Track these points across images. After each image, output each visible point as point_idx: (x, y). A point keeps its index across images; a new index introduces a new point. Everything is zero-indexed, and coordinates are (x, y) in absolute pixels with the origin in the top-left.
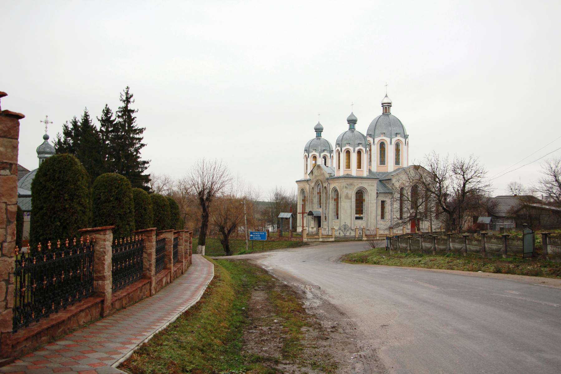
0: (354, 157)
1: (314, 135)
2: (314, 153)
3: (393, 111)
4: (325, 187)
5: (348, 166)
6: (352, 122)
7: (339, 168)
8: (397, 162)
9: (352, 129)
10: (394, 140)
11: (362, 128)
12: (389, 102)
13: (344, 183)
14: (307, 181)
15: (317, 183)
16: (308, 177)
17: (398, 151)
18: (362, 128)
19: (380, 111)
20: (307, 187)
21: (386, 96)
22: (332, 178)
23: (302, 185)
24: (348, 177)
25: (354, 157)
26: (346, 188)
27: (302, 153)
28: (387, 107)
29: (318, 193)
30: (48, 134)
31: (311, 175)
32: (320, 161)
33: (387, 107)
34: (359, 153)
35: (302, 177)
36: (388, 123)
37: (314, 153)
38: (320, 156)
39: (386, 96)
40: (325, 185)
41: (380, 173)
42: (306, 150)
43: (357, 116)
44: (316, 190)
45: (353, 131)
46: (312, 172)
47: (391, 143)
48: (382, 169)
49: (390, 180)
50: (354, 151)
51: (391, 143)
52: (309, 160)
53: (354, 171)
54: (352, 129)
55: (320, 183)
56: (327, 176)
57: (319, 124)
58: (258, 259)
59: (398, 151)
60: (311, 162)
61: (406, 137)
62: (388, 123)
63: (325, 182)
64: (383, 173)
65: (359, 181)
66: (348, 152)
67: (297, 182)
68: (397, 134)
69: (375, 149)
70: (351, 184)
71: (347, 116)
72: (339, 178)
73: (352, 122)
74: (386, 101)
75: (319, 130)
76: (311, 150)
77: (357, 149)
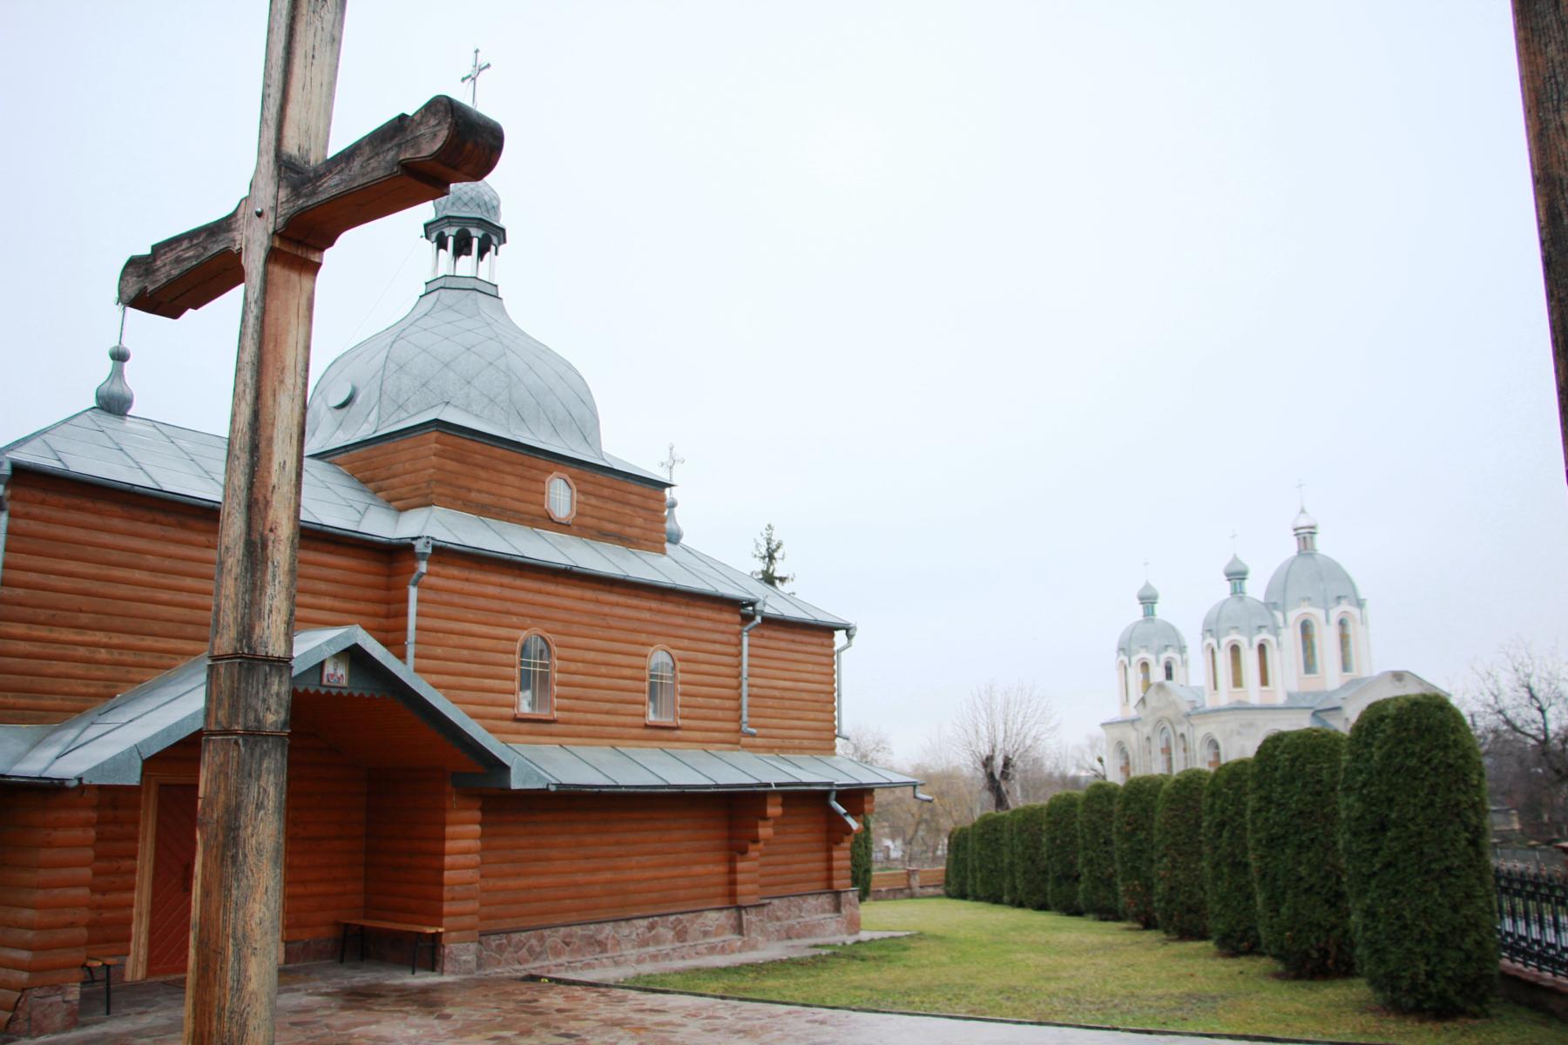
0: (1250, 659)
1: (1138, 612)
2: (1144, 655)
3: (1322, 544)
4: (1182, 736)
5: (1237, 682)
6: (1237, 576)
7: (1216, 688)
8: (1346, 667)
9: (1237, 592)
10: (1335, 614)
11: (1256, 588)
12: (1311, 523)
13: (1233, 722)
14: (1133, 722)
15: (1160, 725)
16: (1133, 713)
17: (1344, 640)
18: (1256, 588)
19: (1291, 547)
20: (1133, 738)
21: (1303, 511)
22: (1196, 713)
23: (1117, 733)
24: (1240, 708)
25: (1250, 659)
26: (1239, 733)
27: (1112, 658)
28: (1305, 536)
29: (1163, 751)
30: (127, 345)
31: (1141, 707)
32: (1158, 674)
33: (1305, 536)
34: (1262, 648)
35: (1115, 713)
36: (1312, 572)
37: (1144, 655)
38: (1158, 661)
39: (1303, 511)
40: (1179, 730)
41: (1308, 693)
42: (1121, 649)
43: (1158, 586)
44: (1158, 744)
45: (1241, 599)
46: (1143, 700)
47: (1327, 621)
48: (1311, 684)
49: (1337, 709)
50: (1251, 645)
51: (1327, 621)
52: (1130, 671)
53: (1253, 692)
54: (1237, 592)
55: (1168, 725)
56: (1187, 708)
57: (1235, 560)
58: (359, 571)
59: (1344, 640)
60: (1135, 675)
61: (1360, 604)
62: (1312, 572)
63: (1180, 723)
64: (1316, 695)
65: (1268, 715)
66: (1145, 665)
67: (1103, 725)
68: (1339, 598)
69: (1291, 637)
70: (1251, 725)
71: (1224, 563)
72: (1217, 711)
73: (1237, 576)
74: (1303, 521)
75: (1148, 600)
76: (1134, 647)
77: (1257, 640)
